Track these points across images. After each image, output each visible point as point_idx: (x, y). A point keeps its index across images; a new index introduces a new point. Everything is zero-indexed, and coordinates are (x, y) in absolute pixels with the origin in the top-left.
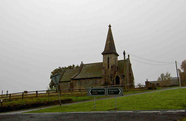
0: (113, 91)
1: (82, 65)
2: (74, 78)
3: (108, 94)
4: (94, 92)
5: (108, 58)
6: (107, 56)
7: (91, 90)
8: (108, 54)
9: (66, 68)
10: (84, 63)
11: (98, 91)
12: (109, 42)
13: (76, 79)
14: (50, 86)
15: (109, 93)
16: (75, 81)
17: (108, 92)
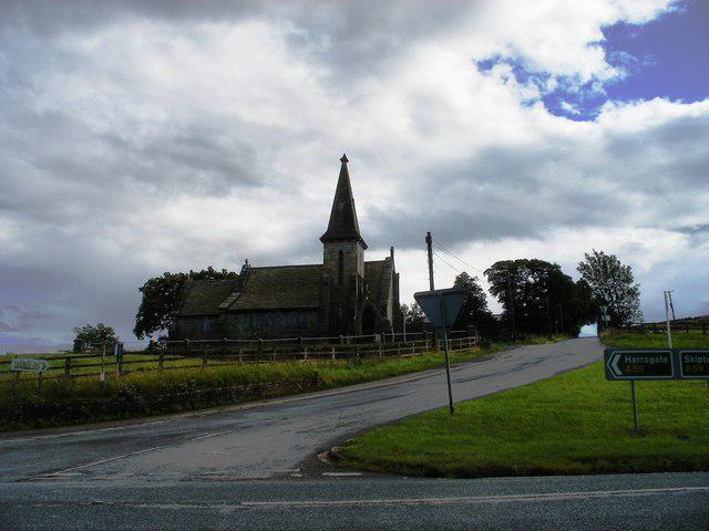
0: (700, 360)
1: (247, 270)
2: (231, 305)
3: (685, 374)
4: (632, 365)
5: (341, 253)
6: (337, 247)
7: (618, 357)
8: (341, 240)
9: (183, 277)
10: (253, 265)
11: (646, 360)
12: (342, 204)
13: (238, 312)
14: (78, 344)
15: (687, 369)
16: (234, 316)
17: (684, 364)
